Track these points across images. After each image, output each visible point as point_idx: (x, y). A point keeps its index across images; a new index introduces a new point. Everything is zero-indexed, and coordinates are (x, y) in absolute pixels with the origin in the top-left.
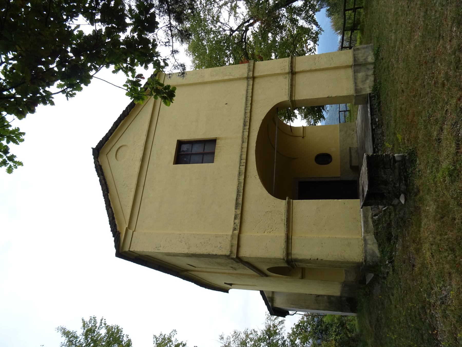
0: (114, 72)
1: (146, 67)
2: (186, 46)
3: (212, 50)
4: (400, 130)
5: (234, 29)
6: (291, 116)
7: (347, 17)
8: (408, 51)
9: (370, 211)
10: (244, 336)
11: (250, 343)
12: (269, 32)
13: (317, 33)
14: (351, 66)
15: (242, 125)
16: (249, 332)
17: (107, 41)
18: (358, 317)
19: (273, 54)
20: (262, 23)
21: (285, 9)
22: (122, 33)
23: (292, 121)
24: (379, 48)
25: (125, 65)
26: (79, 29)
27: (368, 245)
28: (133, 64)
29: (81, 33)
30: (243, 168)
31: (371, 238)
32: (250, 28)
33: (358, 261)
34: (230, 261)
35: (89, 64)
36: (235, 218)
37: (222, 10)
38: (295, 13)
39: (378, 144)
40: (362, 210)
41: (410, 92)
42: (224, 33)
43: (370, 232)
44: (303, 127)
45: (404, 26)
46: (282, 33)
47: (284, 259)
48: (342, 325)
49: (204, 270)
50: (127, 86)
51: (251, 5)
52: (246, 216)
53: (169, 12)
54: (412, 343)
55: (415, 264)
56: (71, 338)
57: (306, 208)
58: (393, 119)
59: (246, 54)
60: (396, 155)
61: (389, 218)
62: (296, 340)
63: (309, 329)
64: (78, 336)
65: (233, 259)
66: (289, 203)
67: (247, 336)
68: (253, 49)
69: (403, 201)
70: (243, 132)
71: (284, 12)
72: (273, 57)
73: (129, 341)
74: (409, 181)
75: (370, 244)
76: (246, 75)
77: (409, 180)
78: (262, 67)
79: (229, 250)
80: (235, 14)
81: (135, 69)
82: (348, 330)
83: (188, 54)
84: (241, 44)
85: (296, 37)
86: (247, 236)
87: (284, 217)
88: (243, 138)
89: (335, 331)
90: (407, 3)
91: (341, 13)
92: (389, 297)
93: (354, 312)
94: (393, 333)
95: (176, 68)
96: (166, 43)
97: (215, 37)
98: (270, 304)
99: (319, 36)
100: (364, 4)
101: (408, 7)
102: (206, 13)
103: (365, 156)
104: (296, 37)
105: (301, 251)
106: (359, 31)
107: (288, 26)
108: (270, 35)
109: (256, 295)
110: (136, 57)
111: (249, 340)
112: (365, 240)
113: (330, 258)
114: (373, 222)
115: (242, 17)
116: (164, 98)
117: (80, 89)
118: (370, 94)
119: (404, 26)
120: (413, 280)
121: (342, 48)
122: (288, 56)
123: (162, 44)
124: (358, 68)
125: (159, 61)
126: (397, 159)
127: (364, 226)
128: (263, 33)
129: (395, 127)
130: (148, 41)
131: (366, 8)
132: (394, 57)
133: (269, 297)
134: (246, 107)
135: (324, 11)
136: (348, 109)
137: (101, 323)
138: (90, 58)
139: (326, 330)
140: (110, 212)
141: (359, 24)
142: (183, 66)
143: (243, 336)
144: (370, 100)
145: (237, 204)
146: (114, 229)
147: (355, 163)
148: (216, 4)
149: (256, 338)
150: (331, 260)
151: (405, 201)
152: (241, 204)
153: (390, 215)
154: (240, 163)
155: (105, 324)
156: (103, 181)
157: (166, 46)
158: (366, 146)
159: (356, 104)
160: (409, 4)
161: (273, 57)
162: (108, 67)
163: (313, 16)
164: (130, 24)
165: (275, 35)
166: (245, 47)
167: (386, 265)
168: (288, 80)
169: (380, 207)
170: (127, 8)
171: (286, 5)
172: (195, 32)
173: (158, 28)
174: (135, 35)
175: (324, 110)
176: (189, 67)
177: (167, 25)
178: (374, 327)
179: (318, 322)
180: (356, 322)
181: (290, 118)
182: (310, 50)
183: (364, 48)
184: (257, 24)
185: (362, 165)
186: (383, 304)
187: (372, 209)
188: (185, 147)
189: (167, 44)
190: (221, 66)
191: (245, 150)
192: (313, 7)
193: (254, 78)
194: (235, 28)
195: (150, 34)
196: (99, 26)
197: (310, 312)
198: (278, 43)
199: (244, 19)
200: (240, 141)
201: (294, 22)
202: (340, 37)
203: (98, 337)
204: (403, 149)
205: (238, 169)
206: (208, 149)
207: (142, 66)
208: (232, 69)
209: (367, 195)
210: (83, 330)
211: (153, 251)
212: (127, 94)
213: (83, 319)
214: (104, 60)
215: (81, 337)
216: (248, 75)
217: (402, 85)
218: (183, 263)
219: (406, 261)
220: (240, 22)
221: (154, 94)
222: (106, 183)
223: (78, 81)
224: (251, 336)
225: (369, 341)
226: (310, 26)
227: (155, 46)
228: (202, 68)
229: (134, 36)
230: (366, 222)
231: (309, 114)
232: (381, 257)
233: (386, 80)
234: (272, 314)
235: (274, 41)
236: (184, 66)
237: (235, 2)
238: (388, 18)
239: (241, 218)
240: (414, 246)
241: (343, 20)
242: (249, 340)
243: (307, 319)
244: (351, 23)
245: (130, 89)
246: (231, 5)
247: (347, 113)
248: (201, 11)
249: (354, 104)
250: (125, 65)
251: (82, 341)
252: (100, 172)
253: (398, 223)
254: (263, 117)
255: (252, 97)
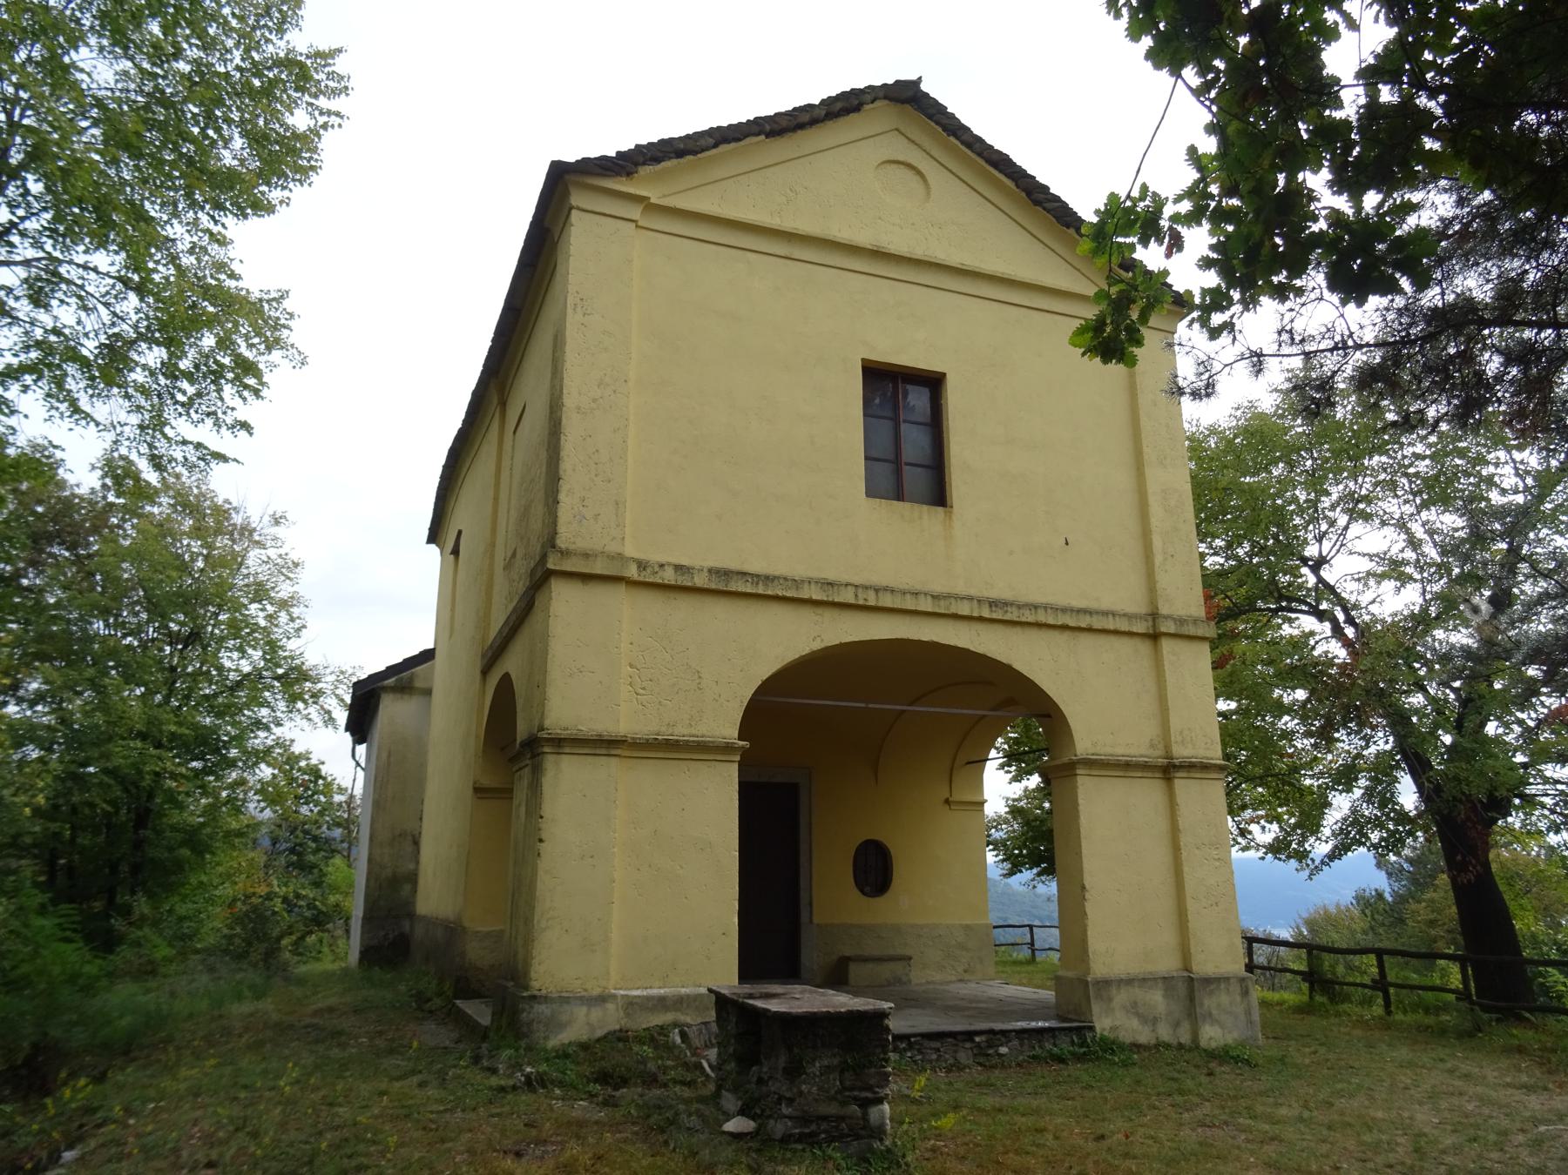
0: (1192, 150)
1: (1206, 263)
2: (1268, 403)
3: (1250, 493)
4: (968, 1126)
5: (1322, 573)
6: (1019, 761)
7: (1356, 960)
8: (1238, 1159)
9: (699, 1020)
10: (283, 595)
11: (261, 614)
12: (1312, 692)
13: (1302, 856)
14: (1187, 969)
15: (994, 594)
16: (296, 611)
17: (1300, 125)
18: (346, 972)
19: (1233, 705)
20: (1343, 666)
21: (1388, 747)
22: (1330, 177)
23: (1002, 767)
24: (1248, 1062)
25: (1214, 189)
26: (1342, 27)
27: (584, 1009)
28: (1220, 216)
29: (1331, 34)
30: (847, 596)
31: (610, 1019)
32: (1326, 627)
33: (533, 975)
34: (537, 549)
35: (1220, 64)
36: (679, 568)
37: (1389, 531)
38: (1375, 780)
39: (920, 1052)
40: (703, 990)
41: (1096, 1163)
42: (1310, 536)
43: (628, 1015)
44: (982, 803)
45: (1325, 1148)
46: (1308, 734)
47: (541, 729)
48: (319, 920)
49: (506, 463)
50: (1142, 199)
51: (1405, 630)
52: (685, 604)
53: (1394, 348)
54: (267, 1140)
55: (524, 1160)
56: (280, 11)
57: (711, 805)
58: (1005, 1102)
59: (1234, 613)
60: (886, 1107)
61: (675, 1082)
62: (269, 765)
63: (304, 810)
64: (286, 37)
65: (544, 557)
66: (727, 748)
67: (284, 604)
68: (1253, 638)
69: (730, 1126)
70: (970, 598)
71: (1381, 742)
72: (1223, 705)
73: (270, 209)
74: (800, 1147)
75: (587, 1015)
76: (1164, 609)
77: (803, 1150)
78: (1191, 667)
79: (572, 547)
80: (1375, 575)
81: (1199, 224)
82: (302, 938)
83: (1239, 413)
84: (1271, 593)
85: (1290, 784)
86: (619, 604)
87: (681, 732)
88: (948, 597)
89: (298, 896)
90: (1403, 1163)
91: (1369, 940)
92: (414, 1072)
93: (361, 960)
94: (298, 1082)
95: (1202, 369)
96: (1290, 332)
97: (1299, 505)
98: (391, 681)
99: (1293, 863)
100: (1399, 1017)
101: (1390, 1166)
102: (1382, 476)
103: (886, 1005)
104: (1290, 784)
105: (568, 785)
106: (1306, 998)
107: (1330, 757)
108: (1301, 694)
109: (421, 636)
110: (1245, 230)
111: (270, 609)
112: (602, 999)
113: (544, 883)
114: (662, 1027)
115: (1364, 599)
116: (1098, 326)
117: (1134, 34)
118: (1092, 1029)
119: (1325, 1148)
120: (471, 1151)
121: (1250, 941)
122: (1227, 757)
123: (1286, 320)
124: (1182, 989)
125: (1228, 308)
126: (874, 1112)
127: (648, 998)
128: (1309, 672)
129: (979, 1110)
130: (1298, 269)
131: (1385, 1025)
132: (1217, 1112)
133: (411, 679)
134: (1056, 609)
135: (1379, 881)
136: (1040, 957)
137: (329, 113)
138: (1242, 69)
139: (304, 867)
140: (702, 142)
141: (1332, 1000)
142: (1206, 391)
143: (284, 590)
144: (1070, 1029)
145: (727, 574)
146: (644, 154)
147: (855, 970)
148: (1412, 510)
149: (277, 633)
150: (539, 885)
151: (731, 1134)
152: (726, 587)
153: (683, 1083)
154: (866, 588)
155: (325, 126)
156: (806, 118)
157: (1279, 333)
158: (913, 1011)
159: (1059, 983)
160: (1399, 1168)
161: (1223, 705)
162: (1211, 129)
163: (1364, 844)
164: (1359, 208)
165: (1302, 712)
166: (1260, 610)
167: (518, 1066)
168: (1143, 751)
169: (713, 1053)
170: (1416, 197)
171: (1403, 752)
172: (1317, 435)
173: (1344, 303)
174: (1321, 225)
175: (1039, 874)
176: (1198, 415)
177: (1351, 335)
178: (315, 1021)
179: (327, 840)
180: (328, 965)
181: (1011, 757)
182: (1243, 833)
183: (1248, 1012)
184: (1339, 652)
185: (856, 993)
186: (391, 1051)
187: (705, 1023)
188: (918, 399)
189: (1285, 337)
190: (1198, 526)
191: (909, 604)
192: (1393, 843)
193: (1154, 637)
194: (1325, 573)
195: (1322, 276)
196: (1351, 103)
197: (363, 814)
198: (1273, 724)
199: (1356, 606)
200: (938, 587)
201: (1345, 777)
202: (1285, 934)
203: (282, 103)
204: (906, 1132)
205: (845, 578)
206: (915, 478)
207: (1212, 248)
208: (1188, 562)
209: (755, 1009)
210: (305, 51)
211: (570, 288)
212: (1113, 197)
213: (340, 51)
214: (1236, 116)
215: (282, 44)
216: (1167, 617)
217: (1121, 1136)
218: (530, 389)
219: (534, 1132)
220: (1349, 590)
221: (1114, 290)
222: (801, 127)
223: (1162, 26)
224: (283, 617)
225: (267, 1005)
226: (1327, 832)
227: (1281, 293)
228: (1191, 459)
229: (1315, 219)
230: (661, 1003)
231: (1027, 823)
232: (546, 1051)
233: (1138, 1082)
234: (358, 685)
235: (1280, 709)
236: (1208, 395)
237: (1418, 577)
238: (1351, 1096)
239: (681, 586)
240: (586, 1159)
241: (1345, 946)
242: (270, 609)
243: (340, 804)
244: (1334, 973)
245: (1132, 209)
246: (1408, 563)
247: (1025, 953)
248: (1390, 457)
249: (1060, 973)
250: (1214, 189)
251: (270, 48)
252: (839, 105)
253: (659, 1107)
254: (1018, 666)
255: (1090, 630)
